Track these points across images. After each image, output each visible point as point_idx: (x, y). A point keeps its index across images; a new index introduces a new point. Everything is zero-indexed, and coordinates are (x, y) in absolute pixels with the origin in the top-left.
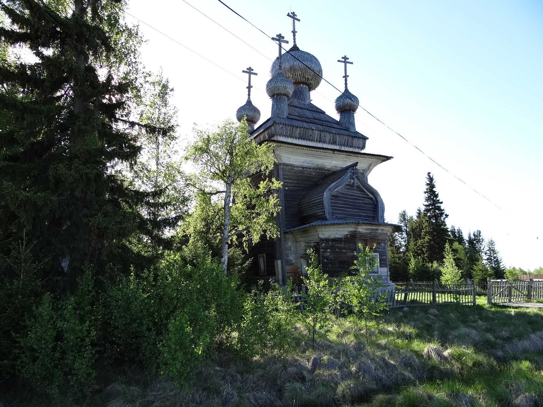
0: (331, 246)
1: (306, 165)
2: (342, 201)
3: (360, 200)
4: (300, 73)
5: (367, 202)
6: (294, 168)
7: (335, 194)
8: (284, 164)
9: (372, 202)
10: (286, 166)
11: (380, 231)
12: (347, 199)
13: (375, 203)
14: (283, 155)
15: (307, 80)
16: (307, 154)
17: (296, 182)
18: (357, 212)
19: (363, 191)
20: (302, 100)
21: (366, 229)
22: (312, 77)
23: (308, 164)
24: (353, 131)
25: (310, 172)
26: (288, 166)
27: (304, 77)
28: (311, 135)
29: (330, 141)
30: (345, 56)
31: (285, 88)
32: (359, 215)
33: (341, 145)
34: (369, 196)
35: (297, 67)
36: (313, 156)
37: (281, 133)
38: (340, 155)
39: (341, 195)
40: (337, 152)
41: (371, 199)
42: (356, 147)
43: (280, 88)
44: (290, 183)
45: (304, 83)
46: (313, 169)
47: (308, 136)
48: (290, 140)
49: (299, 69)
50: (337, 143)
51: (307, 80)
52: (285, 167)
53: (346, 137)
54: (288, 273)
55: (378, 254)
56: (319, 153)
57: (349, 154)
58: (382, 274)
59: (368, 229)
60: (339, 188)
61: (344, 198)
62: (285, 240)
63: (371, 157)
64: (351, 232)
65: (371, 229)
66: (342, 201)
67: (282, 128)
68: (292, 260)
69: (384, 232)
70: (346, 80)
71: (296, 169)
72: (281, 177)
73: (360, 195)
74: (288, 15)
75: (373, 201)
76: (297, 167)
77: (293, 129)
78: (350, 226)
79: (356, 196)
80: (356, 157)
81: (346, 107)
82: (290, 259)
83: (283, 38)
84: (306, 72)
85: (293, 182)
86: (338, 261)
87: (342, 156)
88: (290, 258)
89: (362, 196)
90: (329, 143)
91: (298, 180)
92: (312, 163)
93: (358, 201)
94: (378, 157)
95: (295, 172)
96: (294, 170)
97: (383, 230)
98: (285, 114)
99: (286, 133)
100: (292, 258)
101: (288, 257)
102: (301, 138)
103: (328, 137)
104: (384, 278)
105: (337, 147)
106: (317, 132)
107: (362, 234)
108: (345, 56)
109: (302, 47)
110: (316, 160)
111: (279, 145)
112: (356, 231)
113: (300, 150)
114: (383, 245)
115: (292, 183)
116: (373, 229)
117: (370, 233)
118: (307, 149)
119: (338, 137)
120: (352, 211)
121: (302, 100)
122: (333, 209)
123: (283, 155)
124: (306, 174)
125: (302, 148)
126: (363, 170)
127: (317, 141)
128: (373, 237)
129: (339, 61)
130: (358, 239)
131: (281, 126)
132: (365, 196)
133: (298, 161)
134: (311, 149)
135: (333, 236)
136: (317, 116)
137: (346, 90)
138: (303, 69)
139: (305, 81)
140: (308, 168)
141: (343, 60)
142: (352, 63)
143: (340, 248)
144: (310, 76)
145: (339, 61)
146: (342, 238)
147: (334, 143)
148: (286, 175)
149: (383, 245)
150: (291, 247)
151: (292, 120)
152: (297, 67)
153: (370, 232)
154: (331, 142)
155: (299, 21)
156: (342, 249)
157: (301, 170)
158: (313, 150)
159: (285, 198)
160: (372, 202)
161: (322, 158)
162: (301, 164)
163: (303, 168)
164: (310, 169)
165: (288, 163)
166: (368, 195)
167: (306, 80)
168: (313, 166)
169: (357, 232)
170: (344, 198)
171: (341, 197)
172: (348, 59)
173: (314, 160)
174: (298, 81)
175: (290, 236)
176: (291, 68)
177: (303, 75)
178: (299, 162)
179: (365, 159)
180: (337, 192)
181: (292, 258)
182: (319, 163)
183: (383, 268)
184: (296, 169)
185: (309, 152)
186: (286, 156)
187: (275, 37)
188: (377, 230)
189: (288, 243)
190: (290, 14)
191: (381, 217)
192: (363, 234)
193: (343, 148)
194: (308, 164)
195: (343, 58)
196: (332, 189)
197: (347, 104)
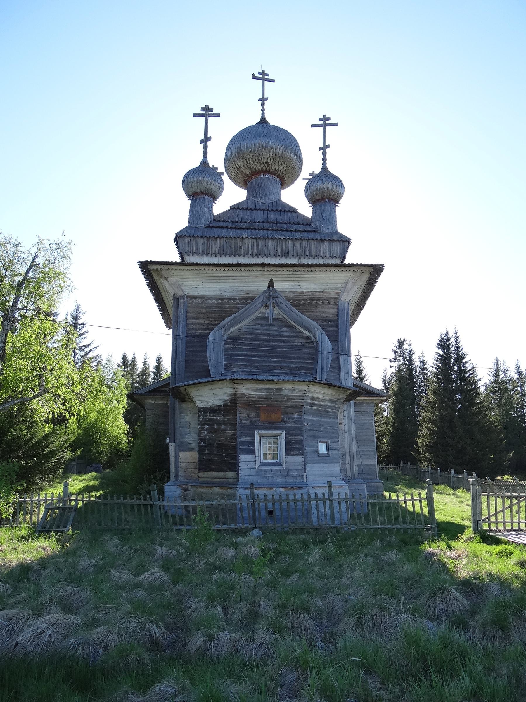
0: (210, 420)
1: (226, 294)
2: (248, 344)
3: (283, 341)
4: (252, 156)
5: (300, 344)
6: (206, 300)
7: (235, 334)
8: (189, 297)
9: (310, 344)
10: (191, 299)
11: (286, 392)
12: (259, 341)
13: (315, 345)
14: (184, 283)
15: (266, 166)
16: (220, 276)
17: (208, 322)
18: (275, 362)
19: (291, 326)
20: (261, 198)
21: (256, 390)
22: (272, 159)
23: (231, 292)
24: (326, 230)
25: (234, 304)
26: (195, 299)
27: (260, 162)
28: (240, 248)
29: (276, 253)
30: (324, 116)
31: (201, 182)
32: (280, 366)
33: (299, 256)
34: (303, 333)
35: (245, 149)
36: (234, 278)
37: (188, 251)
38: (280, 273)
39: (246, 336)
40: (272, 269)
41: (309, 338)
42: (328, 256)
43: (193, 184)
44: (198, 324)
45: (265, 172)
46: (240, 299)
47: (236, 249)
48: (207, 260)
49: (249, 152)
50: (290, 254)
51: (268, 166)
52: (190, 301)
53: (307, 243)
54: (182, 463)
55: (283, 433)
56: (240, 272)
57: (297, 268)
58: (290, 468)
59: (261, 389)
60: (242, 324)
61: (253, 340)
62: (181, 412)
63: (340, 270)
64: (231, 395)
65: (266, 389)
66: (248, 344)
67: (189, 242)
68: (191, 442)
69: (296, 393)
70: (324, 154)
71: (210, 301)
72: (182, 316)
73: (286, 334)
74: (254, 77)
75: (312, 342)
76: (212, 299)
77: (208, 242)
78: (225, 386)
79: (277, 336)
80: (311, 273)
81: (315, 196)
82: (187, 441)
83: (211, 110)
84: (261, 154)
85: (203, 322)
86: (215, 445)
87: (284, 273)
88: (187, 440)
89: (289, 334)
90: (276, 255)
91: (211, 318)
92: (237, 290)
93: (280, 343)
94: (354, 268)
95: (208, 307)
96: (207, 304)
97: (292, 390)
98: (203, 221)
99: (196, 249)
100: (191, 439)
101: (184, 438)
102: (222, 254)
103: (272, 246)
104: (295, 474)
105: (294, 261)
106: (250, 241)
107: (249, 397)
108: (324, 116)
109: (272, 121)
110: (242, 285)
111: (167, 268)
112: (235, 394)
113: (205, 272)
114: (296, 416)
115: (201, 324)
116: (270, 389)
117: (267, 397)
118: (214, 268)
119: (290, 245)
120: (266, 362)
121: (261, 198)
122: (226, 360)
123: (184, 283)
124: (227, 308)
125: (206, 268)
126: (337, 293)
127: (252, 255)
128: (273, 403)
129: (313, 126)
130: (240, 407)
131: (188, 240)
132: (294, 334)
133: (211, 289)
134: (223, 268)
135: (210, 405)
136: (286, 217)
137: (324, 168)
138: (254, 151)
139: (264, 169)
140: (230, 299)
141: (322, 122)
142: (336, 124)
143: (219, 424)
144: (269, 159)
145: (313, 126)
146: (221, 406)
147: (285, 254)
148: (191, 313)
149: (296, 416)
150: (191, 422)
151: (221, 229)
152: (245, 149)
153: (266, 395)
154: (280, 253)
155: (274, 82)
156: (221, 424)
157: (218, 303)
158: (226, 269)
159: (187, 347)
160: (310, 344)
161: (252, 281)
162: (218, 293)
163: (222, 299)
164: (234, 299)
165: (196, 293)
166: (301, 332)
167: (265, 166)
168: (239, 295)
169: (238, 396)
170: (253, 340)
171: (246, 339)
172: (329, 119)
173: (239, 284)
174: (254, 170)
175: (189, 406)
176: (238, 153)
177: (256, 159)
178: (214, 291)
179: (330, 274)
180: (239, 330)
181: (191, 439)
182: (249, 290)
183: (295, 457)
184: (210, 301)
185: (222, 273)
186: (188, 283)
187: (199, 111)
188: (281, 390)
189: (186, 417)
190: (256, 75)
191: (323, 369)
192: (251, 397)
193: (304, 261)
194: (231, 292)
195: (320, 119)
196: (226, 327)
197: (315, 189)
